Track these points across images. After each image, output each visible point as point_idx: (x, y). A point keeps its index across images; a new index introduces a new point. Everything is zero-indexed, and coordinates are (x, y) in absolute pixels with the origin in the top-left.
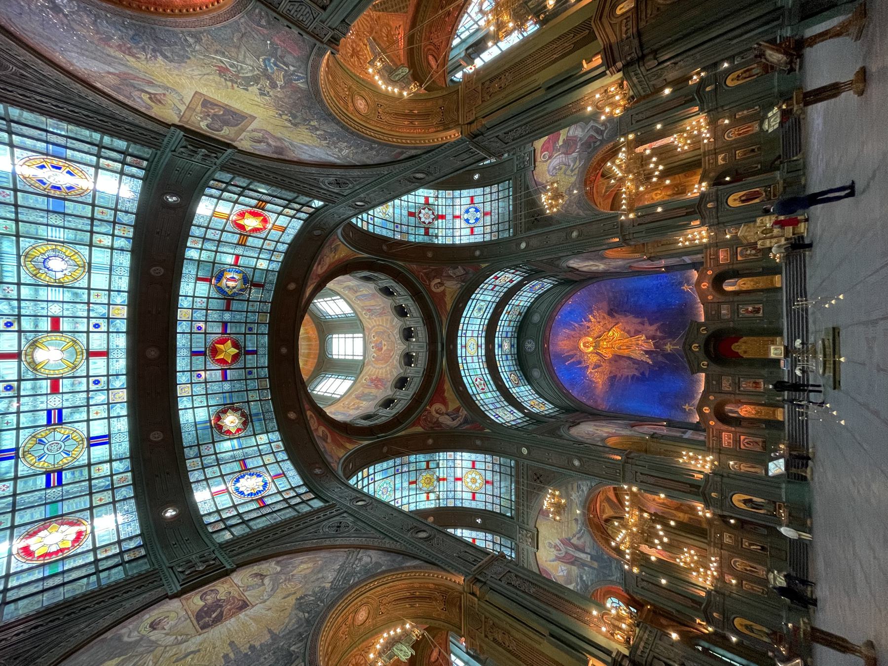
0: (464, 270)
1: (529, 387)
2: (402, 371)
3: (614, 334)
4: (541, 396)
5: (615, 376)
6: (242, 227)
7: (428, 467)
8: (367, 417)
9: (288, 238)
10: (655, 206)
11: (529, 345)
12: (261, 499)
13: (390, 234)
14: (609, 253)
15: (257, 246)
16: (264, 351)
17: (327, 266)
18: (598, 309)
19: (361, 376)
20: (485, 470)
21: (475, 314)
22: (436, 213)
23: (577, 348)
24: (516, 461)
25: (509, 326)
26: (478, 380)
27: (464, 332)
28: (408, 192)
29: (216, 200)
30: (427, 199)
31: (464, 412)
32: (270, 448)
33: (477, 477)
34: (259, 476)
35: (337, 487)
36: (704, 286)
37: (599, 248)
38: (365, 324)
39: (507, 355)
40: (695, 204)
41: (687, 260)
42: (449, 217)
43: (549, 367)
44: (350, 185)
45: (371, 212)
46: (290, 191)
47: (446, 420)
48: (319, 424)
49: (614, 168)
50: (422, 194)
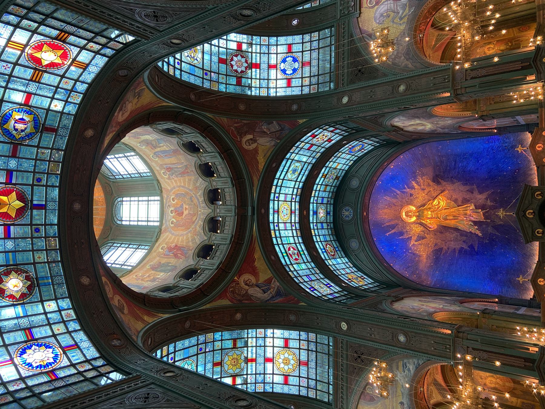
0: (280, 125)
1: (346, 259)
2: (206, 238)
3: (439, 203)
4: (360, 270)
5: (441, 249)
6: (38, 61)
7: (235, 347)
8: (166, 289)
9: (89, 77)
10: (492, 57)
11: (347, 213)
12: (53, 372)
13: (198, 82)
14: (438, 110)
15: (52, 84)
16: (53, 206)
17: (128, 113)
18: (423, 175)
19: (157, 244)
20: (300, 349)
21: (289, 176)
22: (249, 61)
23: (399, 218)
24: (334, 337)
25: (325, 191)
26: (292, 249)
27: (277, 195)
28: (218, 36)
29: (12, 28)
30: (240, 45)
31: (276, 284)
32: (59, 317)
33: (291, 357)
34: (48, 347)
35: (140, 360)
36: (539, 147)
37: (427, 104)
38: (164, 185)
39: (322, 223)
40: (531, 58)
41: (521, 120)
42: (264, 66)
43: (368, 236)
44: (169, 20)
45: (178, 56)
46: (100, 22)
47: (256, 293)
48: (115, 293)
49: (450, 14)
50: (235, 39)
